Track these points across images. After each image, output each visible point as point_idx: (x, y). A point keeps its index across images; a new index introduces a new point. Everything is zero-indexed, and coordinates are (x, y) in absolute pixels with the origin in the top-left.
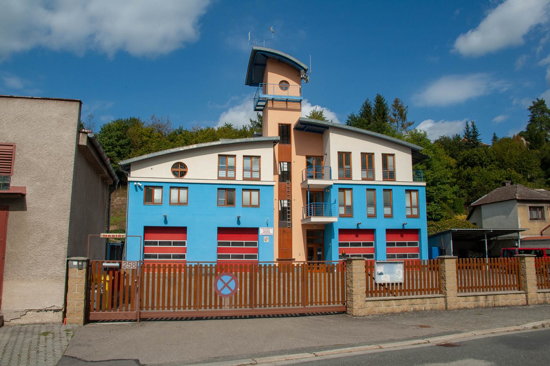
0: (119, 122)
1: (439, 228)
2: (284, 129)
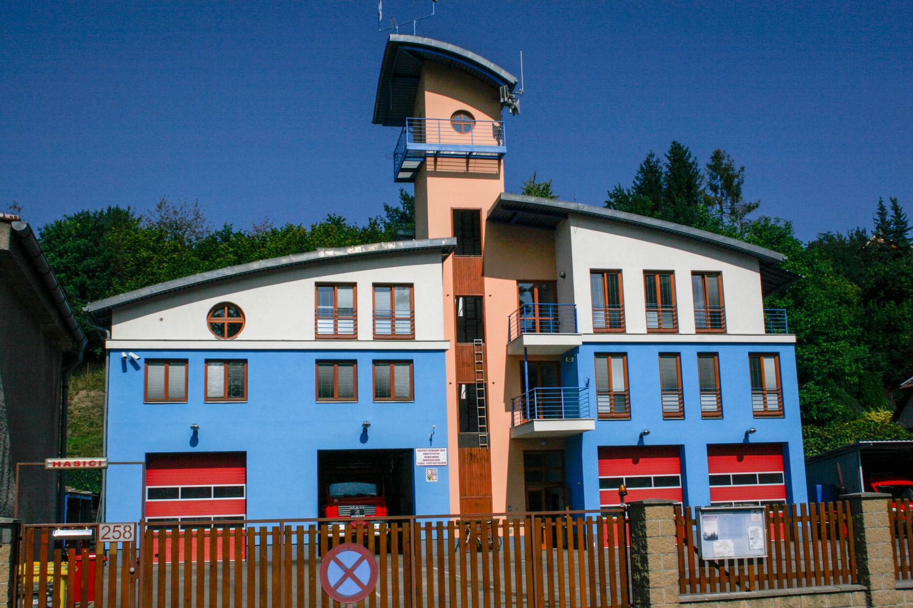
0: (83, 218)
1: (830, 440)
2: (465, 221)
